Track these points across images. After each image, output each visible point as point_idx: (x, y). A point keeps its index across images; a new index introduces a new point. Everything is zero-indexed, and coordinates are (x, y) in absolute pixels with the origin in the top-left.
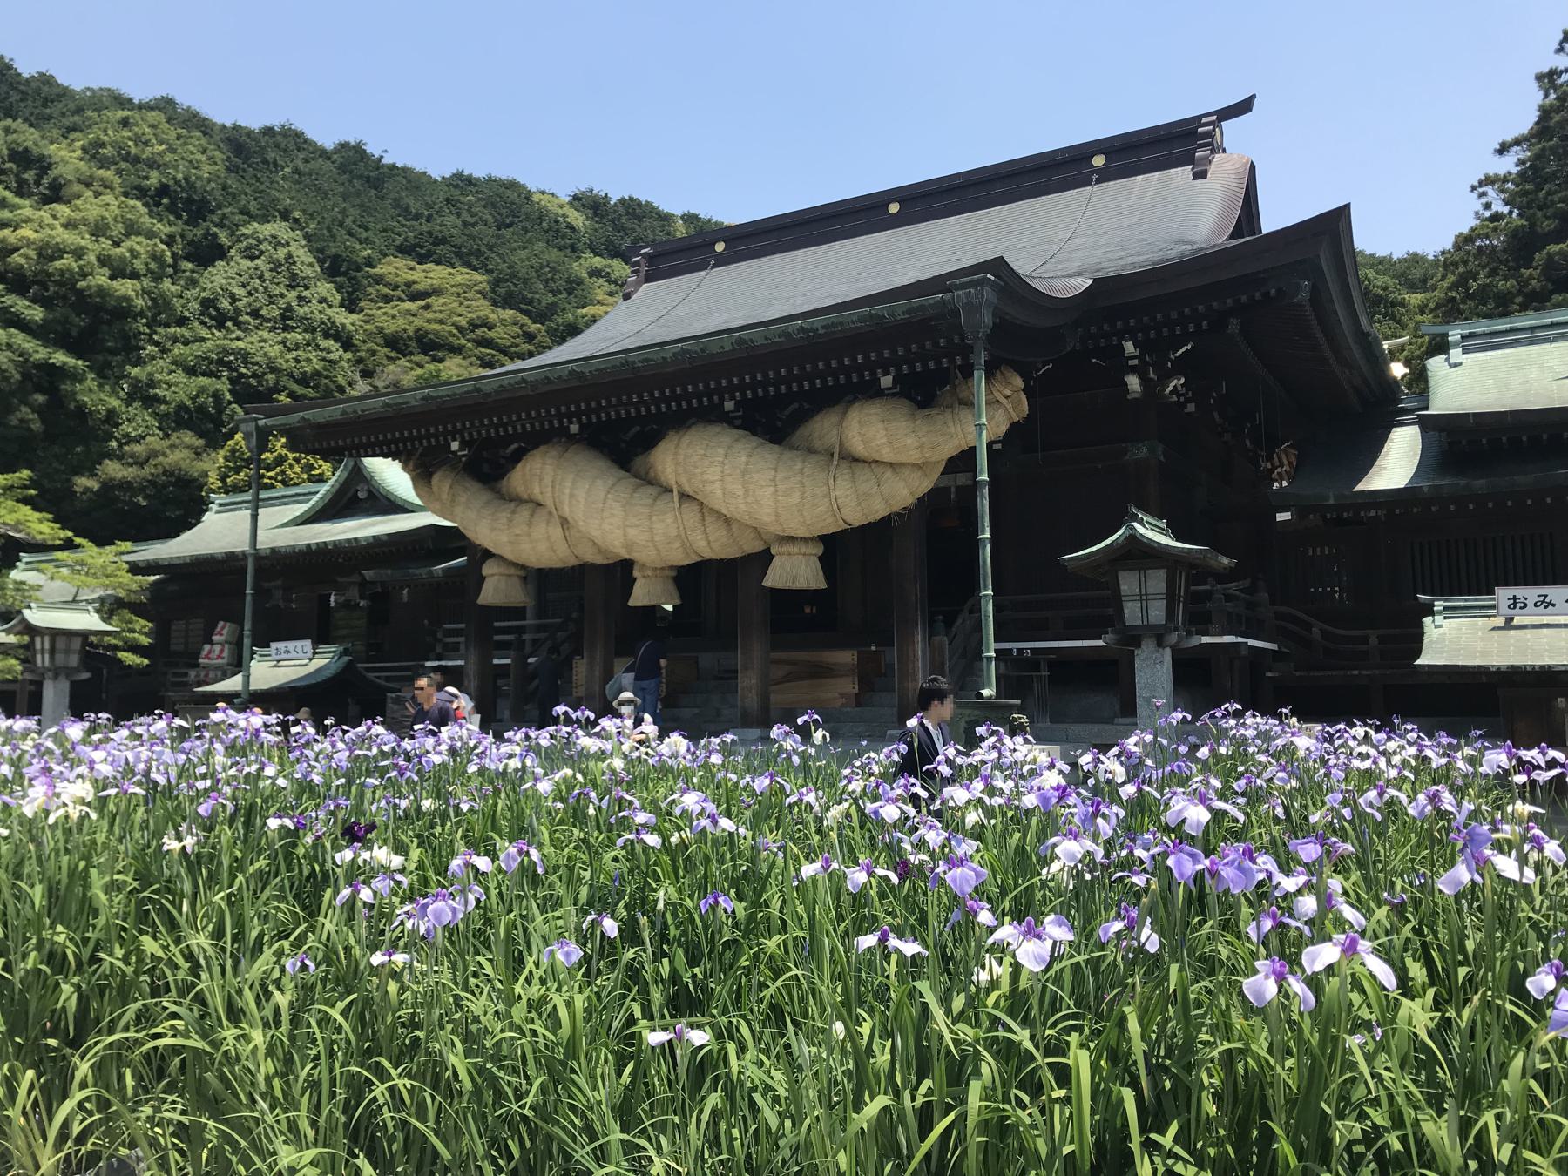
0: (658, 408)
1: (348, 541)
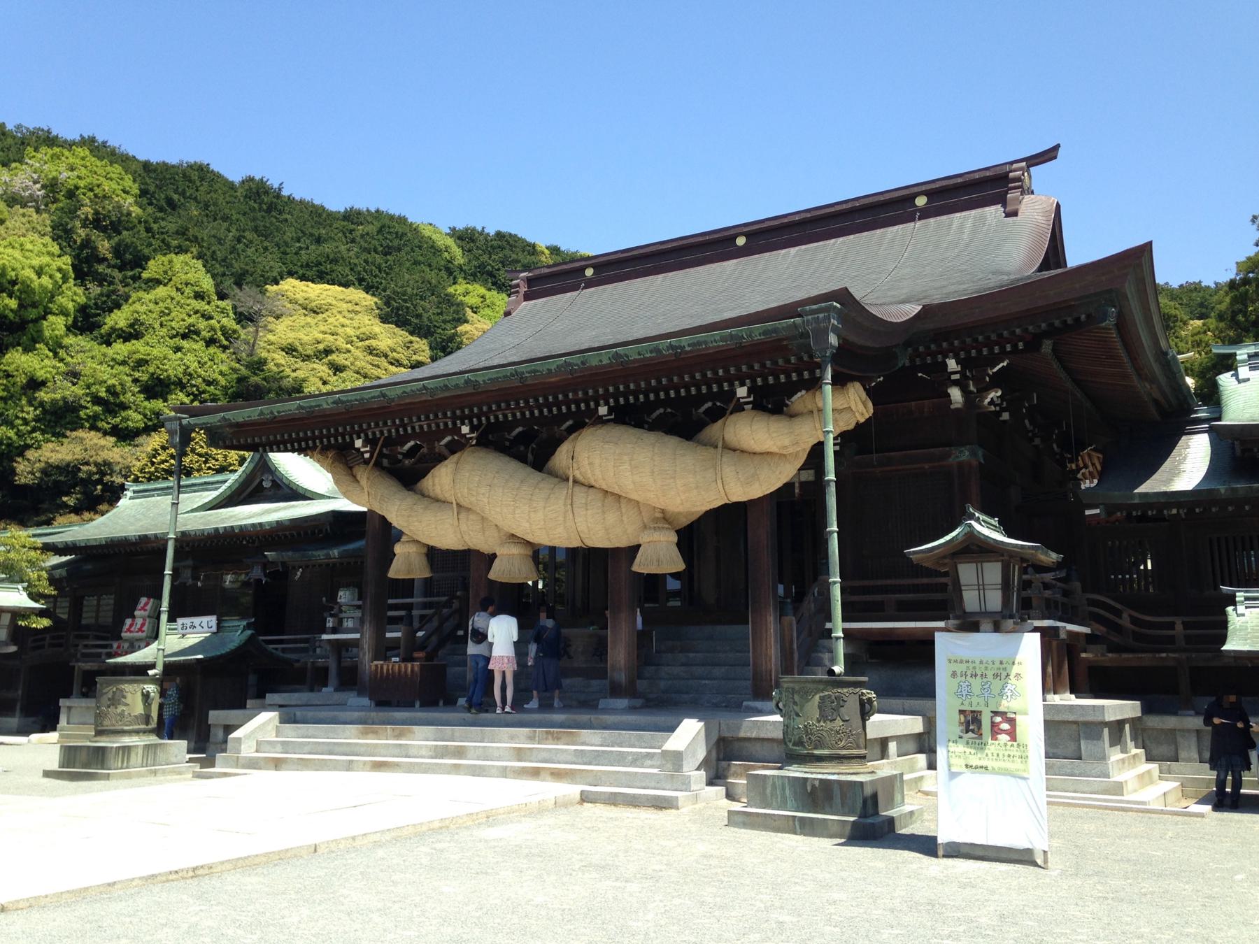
0: (541, 412)
1: (253, 525)
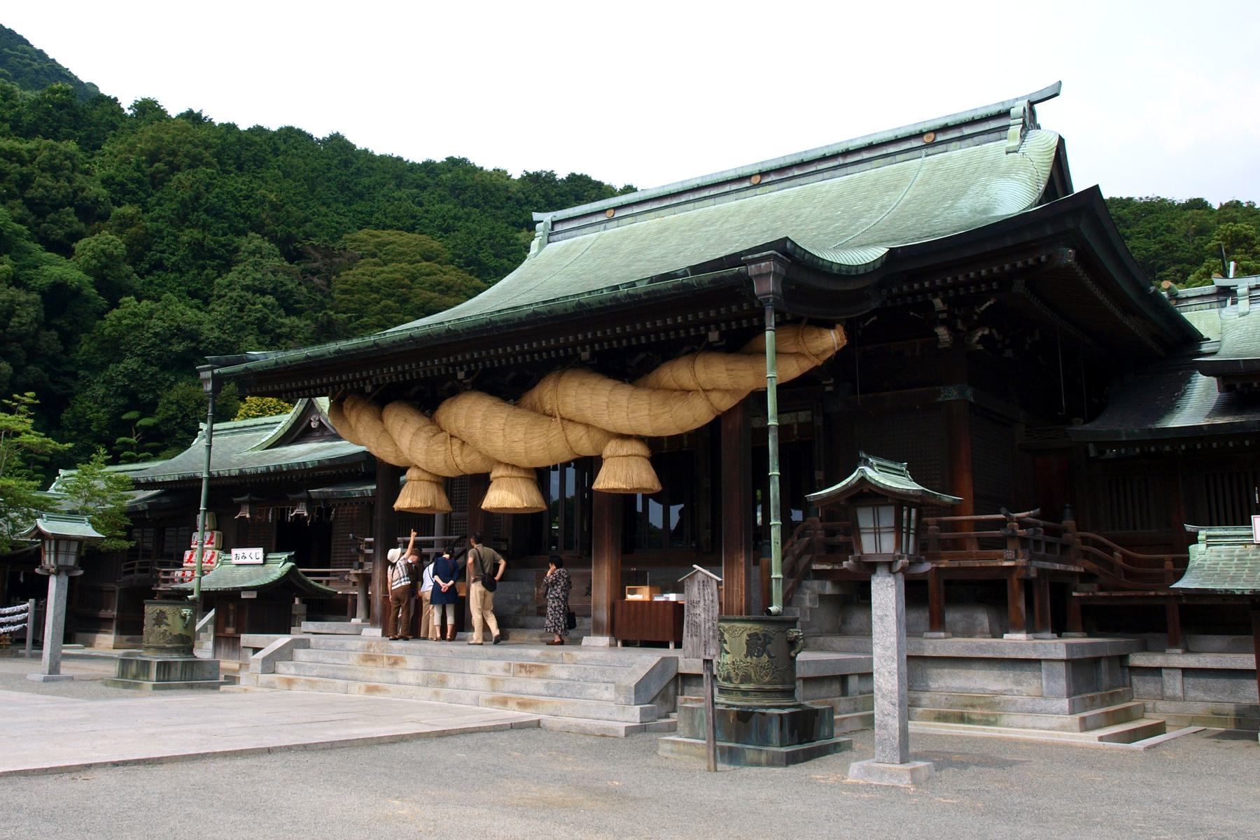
1: (299, 464)
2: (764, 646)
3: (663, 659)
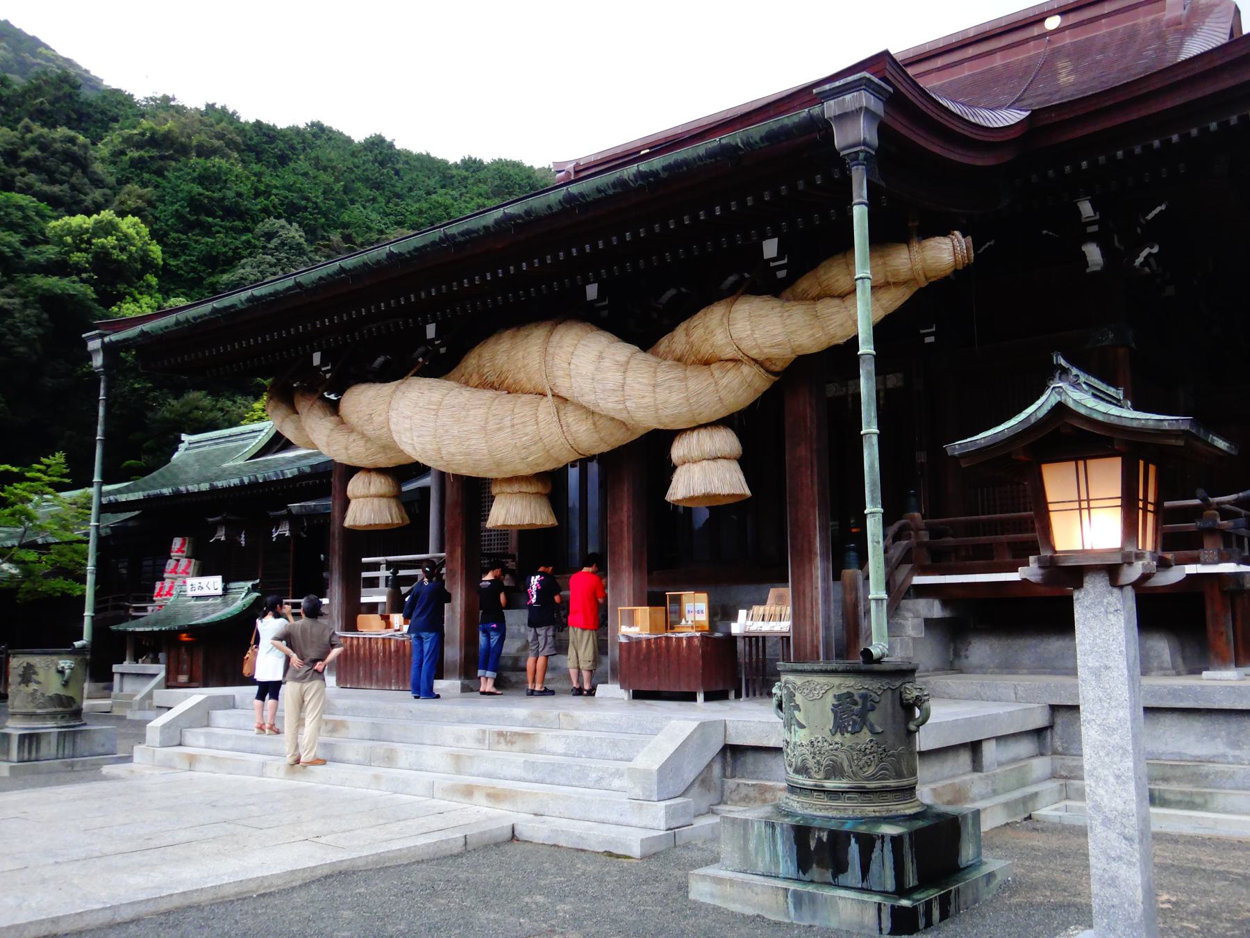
2: (863, 715)
3: (703, 725)
